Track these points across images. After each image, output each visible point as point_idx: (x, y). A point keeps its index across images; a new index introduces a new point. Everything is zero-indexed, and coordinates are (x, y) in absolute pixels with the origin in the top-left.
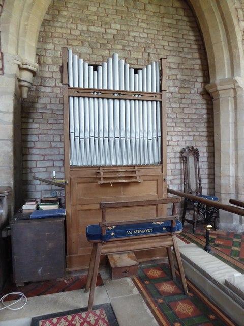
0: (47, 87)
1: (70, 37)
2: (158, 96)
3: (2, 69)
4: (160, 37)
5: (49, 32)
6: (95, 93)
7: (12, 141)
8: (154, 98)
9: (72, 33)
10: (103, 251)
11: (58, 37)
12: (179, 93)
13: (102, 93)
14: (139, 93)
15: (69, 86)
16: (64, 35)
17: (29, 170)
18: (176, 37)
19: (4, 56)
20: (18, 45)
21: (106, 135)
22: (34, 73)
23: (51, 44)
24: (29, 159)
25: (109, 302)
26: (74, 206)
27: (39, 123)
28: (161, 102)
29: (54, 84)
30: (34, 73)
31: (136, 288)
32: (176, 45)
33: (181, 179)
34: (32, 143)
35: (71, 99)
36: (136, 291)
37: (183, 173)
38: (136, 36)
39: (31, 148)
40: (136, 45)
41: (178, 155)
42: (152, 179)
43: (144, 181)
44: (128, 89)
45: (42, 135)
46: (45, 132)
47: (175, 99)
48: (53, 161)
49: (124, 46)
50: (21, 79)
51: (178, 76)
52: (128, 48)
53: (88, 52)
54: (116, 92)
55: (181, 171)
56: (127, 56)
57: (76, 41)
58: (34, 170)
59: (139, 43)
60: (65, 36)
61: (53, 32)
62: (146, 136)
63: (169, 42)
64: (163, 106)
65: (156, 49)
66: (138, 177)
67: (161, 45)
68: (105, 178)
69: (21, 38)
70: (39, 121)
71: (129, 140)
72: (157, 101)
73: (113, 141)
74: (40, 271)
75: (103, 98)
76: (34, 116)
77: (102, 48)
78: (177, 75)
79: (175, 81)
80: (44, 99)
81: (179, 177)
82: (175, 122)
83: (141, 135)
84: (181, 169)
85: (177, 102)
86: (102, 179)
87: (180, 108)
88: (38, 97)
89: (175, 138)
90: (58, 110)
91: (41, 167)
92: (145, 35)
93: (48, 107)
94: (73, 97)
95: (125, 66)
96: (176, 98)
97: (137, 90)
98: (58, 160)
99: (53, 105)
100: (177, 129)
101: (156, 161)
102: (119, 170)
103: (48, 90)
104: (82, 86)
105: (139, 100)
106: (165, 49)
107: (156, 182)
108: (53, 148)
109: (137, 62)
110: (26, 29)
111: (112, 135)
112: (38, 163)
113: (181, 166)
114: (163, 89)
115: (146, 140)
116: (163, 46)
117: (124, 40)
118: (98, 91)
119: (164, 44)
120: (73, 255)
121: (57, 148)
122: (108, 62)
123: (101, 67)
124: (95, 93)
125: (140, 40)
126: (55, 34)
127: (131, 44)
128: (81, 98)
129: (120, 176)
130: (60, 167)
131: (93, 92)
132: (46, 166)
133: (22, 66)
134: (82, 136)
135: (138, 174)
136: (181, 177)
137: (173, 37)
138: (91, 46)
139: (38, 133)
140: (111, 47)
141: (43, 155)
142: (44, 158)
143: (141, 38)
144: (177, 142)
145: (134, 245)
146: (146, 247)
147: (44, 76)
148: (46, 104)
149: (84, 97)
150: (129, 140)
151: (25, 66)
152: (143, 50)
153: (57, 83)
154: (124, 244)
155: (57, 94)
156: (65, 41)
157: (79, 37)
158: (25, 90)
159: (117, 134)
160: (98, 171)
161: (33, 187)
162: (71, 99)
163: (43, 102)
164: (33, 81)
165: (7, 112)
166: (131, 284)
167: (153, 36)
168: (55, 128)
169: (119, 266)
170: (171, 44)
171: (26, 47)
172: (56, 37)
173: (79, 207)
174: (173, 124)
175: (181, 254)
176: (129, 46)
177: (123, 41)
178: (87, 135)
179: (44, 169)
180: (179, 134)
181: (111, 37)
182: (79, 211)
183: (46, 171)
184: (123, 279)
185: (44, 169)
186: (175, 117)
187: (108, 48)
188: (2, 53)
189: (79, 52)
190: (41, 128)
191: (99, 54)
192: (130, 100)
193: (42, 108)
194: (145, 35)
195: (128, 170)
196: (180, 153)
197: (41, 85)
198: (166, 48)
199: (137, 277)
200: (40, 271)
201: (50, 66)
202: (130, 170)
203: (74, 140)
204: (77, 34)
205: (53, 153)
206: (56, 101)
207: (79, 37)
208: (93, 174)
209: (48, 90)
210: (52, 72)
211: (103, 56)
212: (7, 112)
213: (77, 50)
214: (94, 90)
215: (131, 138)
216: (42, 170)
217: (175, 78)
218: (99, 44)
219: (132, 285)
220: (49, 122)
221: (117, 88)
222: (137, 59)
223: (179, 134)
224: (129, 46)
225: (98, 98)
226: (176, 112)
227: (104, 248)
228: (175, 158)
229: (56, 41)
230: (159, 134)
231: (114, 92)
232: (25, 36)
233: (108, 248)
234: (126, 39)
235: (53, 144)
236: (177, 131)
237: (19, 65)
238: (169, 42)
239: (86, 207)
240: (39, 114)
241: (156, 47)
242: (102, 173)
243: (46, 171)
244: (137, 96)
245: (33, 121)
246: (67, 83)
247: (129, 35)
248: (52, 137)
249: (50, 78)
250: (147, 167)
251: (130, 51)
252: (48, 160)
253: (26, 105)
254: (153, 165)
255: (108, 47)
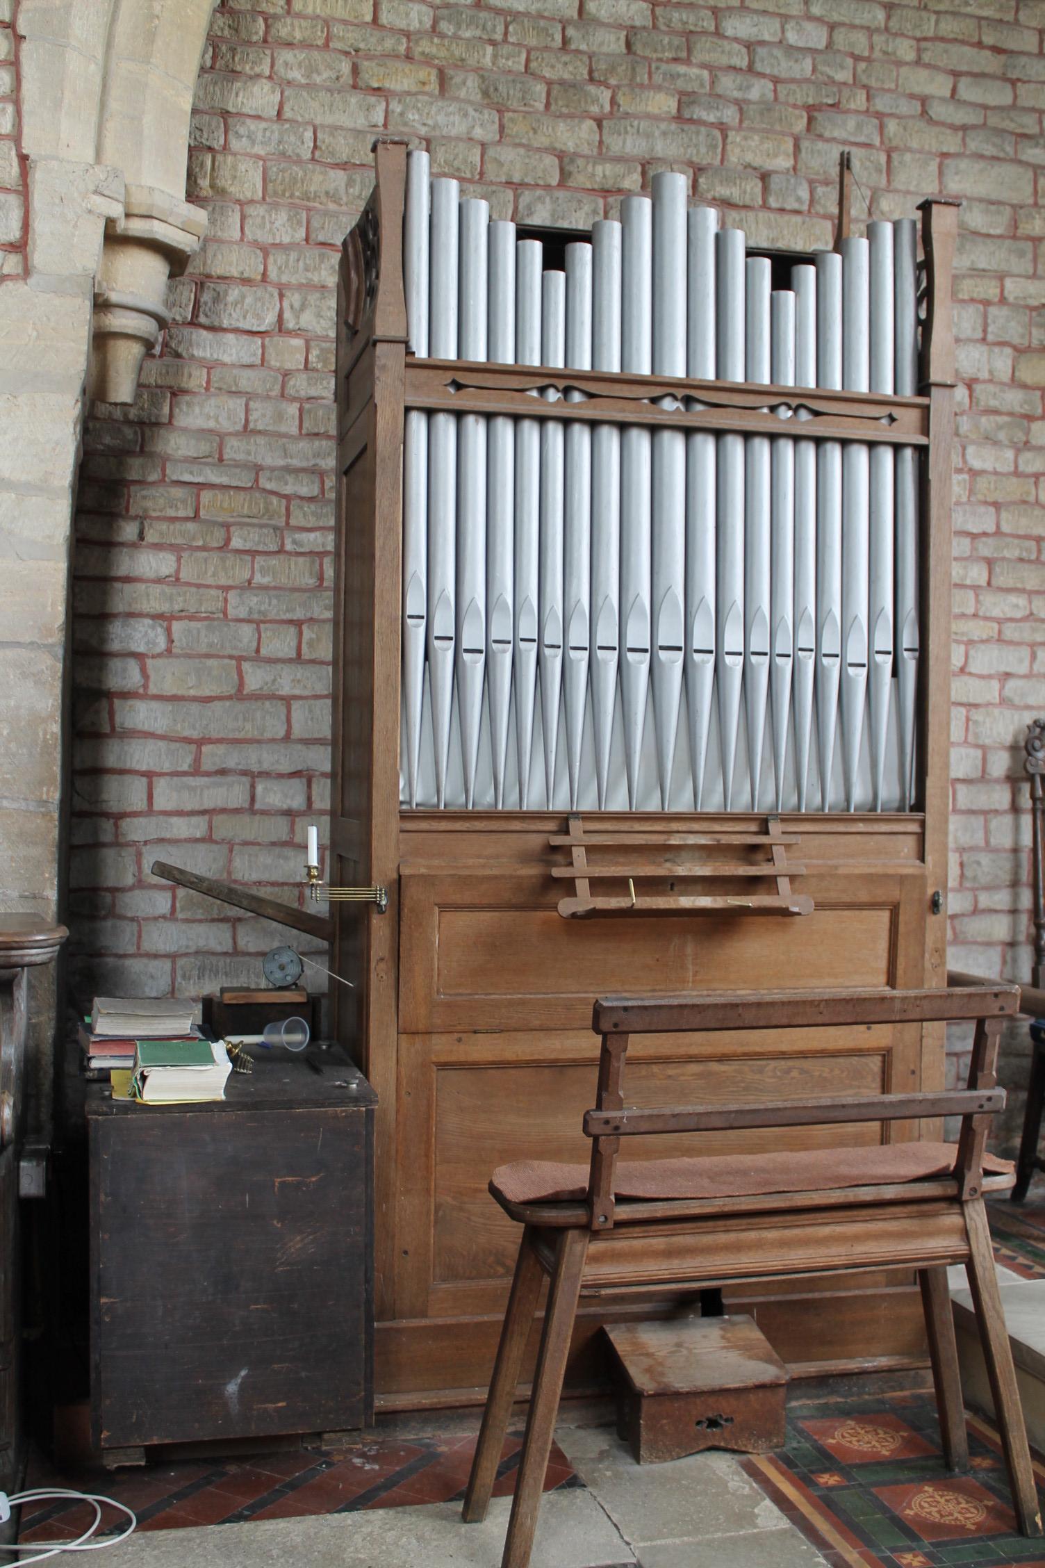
0: (230, 337)
1: (371, 42)
2: (909, 418)
3: (20, 247)
4: (905, 50)
5: (255, 13)
6: (553, 396)
7: (60, 652)
8: (881, 431)
9: (384, 18)
10: (591, 1272)
11: (306, 45)
12: (1015, 383)
13: (591, 396)
14: (799, 400)
15: (410, 353)
16: (337, 30)
17: (108, 825)
18: (997, 50)
19: (38, 177)
20: (103, 105)
21: (606, 634)
22: (176, 260)
23: (266, 86)
24: (111, 760)
25: (634, 1560)
26: (418, 1039)
27: (175, 549)
28: (922, 452)
29: (270, 319)
30: (176, 260)
31: (768, 1502)
32: (1000, 96)
33: (1014, 912)
34: (133, 668)
35: (418, 423)
36: (769, 1517)
37: (1025, 875)
38: (762, 43)
39: (126, 695)
40: (759, 90)
41: (1000, 764)
42: (864, 897)
43: (820, 906)
44: (737, 375)
45: (191, 618)
46: (211, 602)
47: (985, 421)
48: (253, 776)
49: (686, 99)
50: (114, 297)
51: (1008, 283)
52: (709, 108)
53: (478, 133)
54: (671, 387)
55: (1017, 867)
56: (704, 156)
57: (407, 67)
58: (136, 830)
59: (776, 81)
60: (347, 37)
61: (275, 17)
62: (831, 643)
63: (956, 74)
64: (933, 475)
65: (880, 116)
66: (783, 884)
67: (912, 96)
68: (599, 885)
69: (123, 68)
70: (175, 533)
71: (734, 664)
72: (897, 448)
73: (645, 668)
74: (232, 1388)
75: (593, 424)
76: (149, 504)
77: (559, 106)
78: (1001, 277)
79: (993, 311)
80: (211, 407)
81: (1002, 899)
82: (990, 562)
83: (806, 639)
84: (1016, 850)
85: (1002, 436)
86: (582, 886)
87: (1016, 473)
88: (177, 393)
89: (985, 661)
90: (288, 470)
91: (180, 813)
92: (816, 37)
93: (235, 449)
94: (430, 413)
95: (720, 242)
96: (996, 412)
97: (789, 382)
98: (281, 776)
99: (261, 440)
100: (999, 606)
101: (889, 791)
102: (675, 841)
103: (232, 350)
104: (478, 355)
105: (797, 439)
106: (931, 121)
107: (885, 916)
108: (256, 697)
109: (766, 190)
110: (152, 16)
111: (638, 635)
112: (161, 785)
113: (1017, 828)
114: (935, 376)
115: (833, 666)
116: (924, 100)
117: (688, 62)
118: (568, 381)
119: (928, 90)
120: (404, 1323)
121: (273, 697)
122: (625, 220)
123: (588, 247)
124: (553, 396)
125: (785, 67)
126: (283, 30)
127: (728, 84)
128: (470, 420)
129: (681, 871)
130: (289, 813)
131: (542, 390)
132: (208, 805)
133: (123, 226)
134: (473, 636)
135: (781, 864)
136: (1016, 897)
137: (980, 45)
138: (491, 98)
139: (164, 608)
140: (613, 101)
141: (187, 740)
142: (197, 760)
143: (792, 51)
144: (995, 684)
145: (758, 1245)
146: (822, 1262)
147: (218, 269)
148: (220, 437)
149: (489, 416)
150: (734, 664)
151: (137, 227)
152: (800, 125)
153: (287, 315)
154: (723, 1238)
155: (286, 374)
156: (345, 67)
157: (425, 46)
158: (126, 356)
159: (671, 633)
160: (558, 840)
161: (129, 930)
162: (418, 423)
163: (200, 423)
164: (169, 304)
165: (41, 488)
166: (741, 1484)
167: (860, 42)
168: (265, 580)
169: (681, 1385)
170: (968, 91)
171: (148, 120)
172: (290, 45)
173: (443, 1048)
174: (978, 574)
175: (1015, 1343)
176: (717, 97)
177: (682, 69)
178: (502, 629)
179: (196, 828)
180: (1010, 632)
181: (612, 43)
182: (444, 1066)
183: (208, 839)
184: (699, 1459)
185: (196, 828)
186: (991, 528)
187: (595, 109)
188: (23, 159)
189: (423, 131)
190: (184, 576)
191: (542, 141)
192: (747, 436)
193: (195, 460)
194: (816, 37)
195: (725, 839)
196: (1014, 748)
197: (193, 323)
198: (939, 111)
199: (771, 1460)
200: (232, 1388)
201: (250, 210)
202: (737, 840)
203: (427, 657)
204: (415, 25)
205: (250, 731)
206: (279, 417)
207: (425, 46)
208: (525, 858)
209: (232, 350)
210: (265, 251)
211: (561, 155)
212: (41, 488)
213: (412, 116)
214: (545, 378)
215: (746, 654)
216: (182, 828)
217: (992, 292)
218: (540, 89)
219: (747, 1491)
220: (236, 543)
221: (678, 370)
222: (765, 177)
223: (1010, 632)
224: (717, 97)
225: (567, 422)
226: (999, 497)
227: (596, 1259)
228: (983, 778)
229: (291, 64)
230: (909, 638)
231: (657, 392)
232: (146, 59)
233: (616, 1256)
234: (698, 57)
235: (255, 679)
236: (996, 613)
237: (110, 223)
238: (956, 74)
239: (483, 1049)
240: (178, 492)
241: (880, 104)
242: (579, 854)
243: (208, 839)
244: (784, 413)
245: (141, 536)
246: (401, 334)
247: (718, 33)
248: (247, 631)
249: (246, 281)
250: (841, 827)
251: (723, 128)
252: (223, 772)
253: (107, 440)
254: (871, 813)
255: (595, 100)
